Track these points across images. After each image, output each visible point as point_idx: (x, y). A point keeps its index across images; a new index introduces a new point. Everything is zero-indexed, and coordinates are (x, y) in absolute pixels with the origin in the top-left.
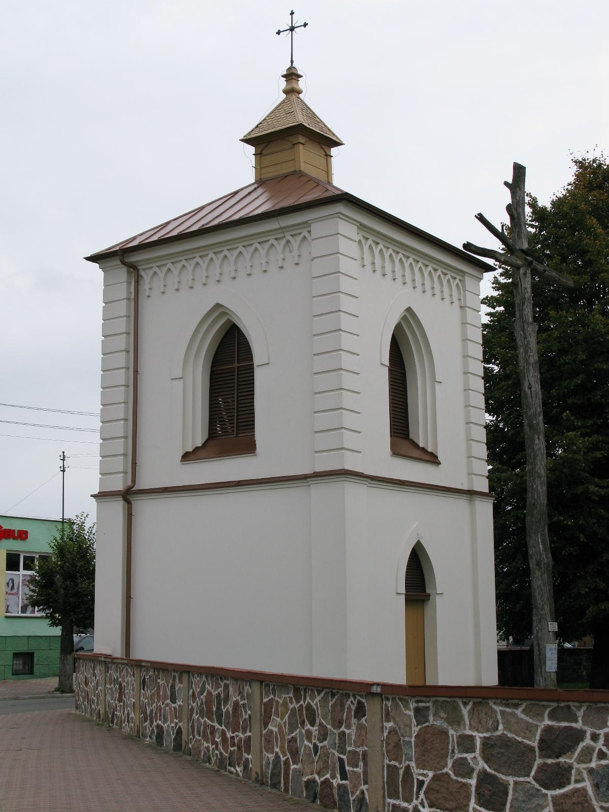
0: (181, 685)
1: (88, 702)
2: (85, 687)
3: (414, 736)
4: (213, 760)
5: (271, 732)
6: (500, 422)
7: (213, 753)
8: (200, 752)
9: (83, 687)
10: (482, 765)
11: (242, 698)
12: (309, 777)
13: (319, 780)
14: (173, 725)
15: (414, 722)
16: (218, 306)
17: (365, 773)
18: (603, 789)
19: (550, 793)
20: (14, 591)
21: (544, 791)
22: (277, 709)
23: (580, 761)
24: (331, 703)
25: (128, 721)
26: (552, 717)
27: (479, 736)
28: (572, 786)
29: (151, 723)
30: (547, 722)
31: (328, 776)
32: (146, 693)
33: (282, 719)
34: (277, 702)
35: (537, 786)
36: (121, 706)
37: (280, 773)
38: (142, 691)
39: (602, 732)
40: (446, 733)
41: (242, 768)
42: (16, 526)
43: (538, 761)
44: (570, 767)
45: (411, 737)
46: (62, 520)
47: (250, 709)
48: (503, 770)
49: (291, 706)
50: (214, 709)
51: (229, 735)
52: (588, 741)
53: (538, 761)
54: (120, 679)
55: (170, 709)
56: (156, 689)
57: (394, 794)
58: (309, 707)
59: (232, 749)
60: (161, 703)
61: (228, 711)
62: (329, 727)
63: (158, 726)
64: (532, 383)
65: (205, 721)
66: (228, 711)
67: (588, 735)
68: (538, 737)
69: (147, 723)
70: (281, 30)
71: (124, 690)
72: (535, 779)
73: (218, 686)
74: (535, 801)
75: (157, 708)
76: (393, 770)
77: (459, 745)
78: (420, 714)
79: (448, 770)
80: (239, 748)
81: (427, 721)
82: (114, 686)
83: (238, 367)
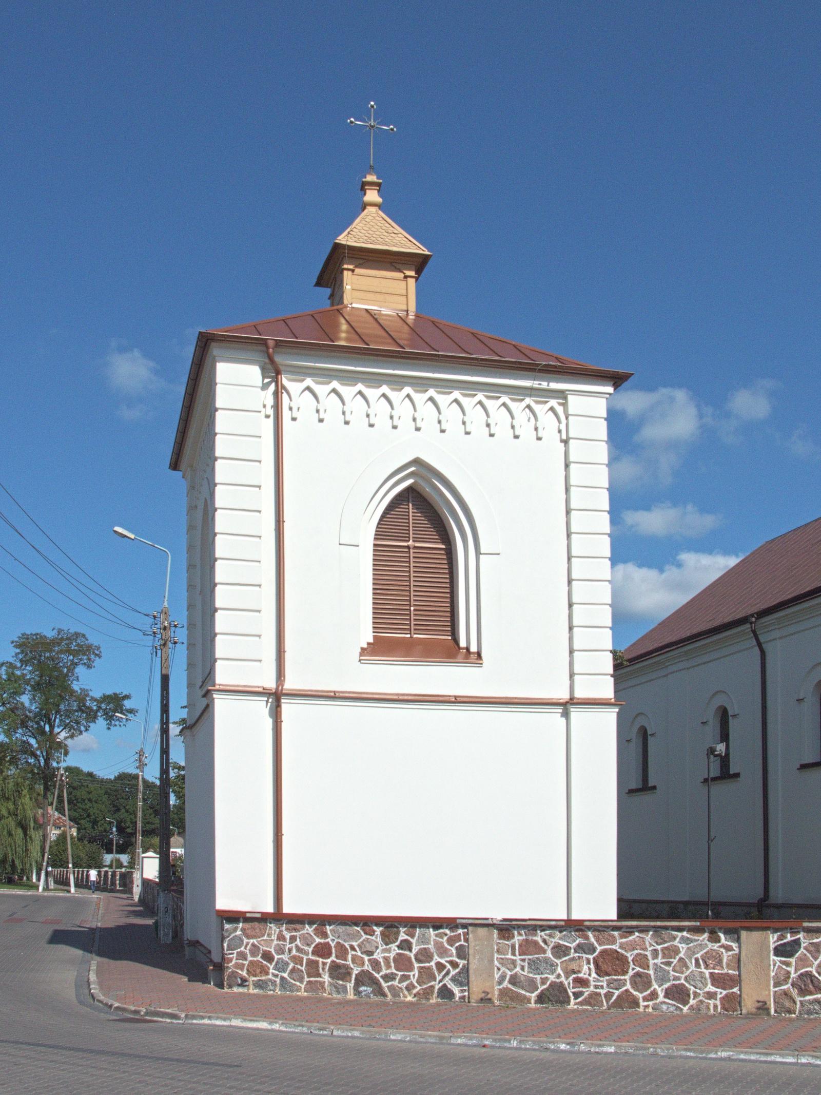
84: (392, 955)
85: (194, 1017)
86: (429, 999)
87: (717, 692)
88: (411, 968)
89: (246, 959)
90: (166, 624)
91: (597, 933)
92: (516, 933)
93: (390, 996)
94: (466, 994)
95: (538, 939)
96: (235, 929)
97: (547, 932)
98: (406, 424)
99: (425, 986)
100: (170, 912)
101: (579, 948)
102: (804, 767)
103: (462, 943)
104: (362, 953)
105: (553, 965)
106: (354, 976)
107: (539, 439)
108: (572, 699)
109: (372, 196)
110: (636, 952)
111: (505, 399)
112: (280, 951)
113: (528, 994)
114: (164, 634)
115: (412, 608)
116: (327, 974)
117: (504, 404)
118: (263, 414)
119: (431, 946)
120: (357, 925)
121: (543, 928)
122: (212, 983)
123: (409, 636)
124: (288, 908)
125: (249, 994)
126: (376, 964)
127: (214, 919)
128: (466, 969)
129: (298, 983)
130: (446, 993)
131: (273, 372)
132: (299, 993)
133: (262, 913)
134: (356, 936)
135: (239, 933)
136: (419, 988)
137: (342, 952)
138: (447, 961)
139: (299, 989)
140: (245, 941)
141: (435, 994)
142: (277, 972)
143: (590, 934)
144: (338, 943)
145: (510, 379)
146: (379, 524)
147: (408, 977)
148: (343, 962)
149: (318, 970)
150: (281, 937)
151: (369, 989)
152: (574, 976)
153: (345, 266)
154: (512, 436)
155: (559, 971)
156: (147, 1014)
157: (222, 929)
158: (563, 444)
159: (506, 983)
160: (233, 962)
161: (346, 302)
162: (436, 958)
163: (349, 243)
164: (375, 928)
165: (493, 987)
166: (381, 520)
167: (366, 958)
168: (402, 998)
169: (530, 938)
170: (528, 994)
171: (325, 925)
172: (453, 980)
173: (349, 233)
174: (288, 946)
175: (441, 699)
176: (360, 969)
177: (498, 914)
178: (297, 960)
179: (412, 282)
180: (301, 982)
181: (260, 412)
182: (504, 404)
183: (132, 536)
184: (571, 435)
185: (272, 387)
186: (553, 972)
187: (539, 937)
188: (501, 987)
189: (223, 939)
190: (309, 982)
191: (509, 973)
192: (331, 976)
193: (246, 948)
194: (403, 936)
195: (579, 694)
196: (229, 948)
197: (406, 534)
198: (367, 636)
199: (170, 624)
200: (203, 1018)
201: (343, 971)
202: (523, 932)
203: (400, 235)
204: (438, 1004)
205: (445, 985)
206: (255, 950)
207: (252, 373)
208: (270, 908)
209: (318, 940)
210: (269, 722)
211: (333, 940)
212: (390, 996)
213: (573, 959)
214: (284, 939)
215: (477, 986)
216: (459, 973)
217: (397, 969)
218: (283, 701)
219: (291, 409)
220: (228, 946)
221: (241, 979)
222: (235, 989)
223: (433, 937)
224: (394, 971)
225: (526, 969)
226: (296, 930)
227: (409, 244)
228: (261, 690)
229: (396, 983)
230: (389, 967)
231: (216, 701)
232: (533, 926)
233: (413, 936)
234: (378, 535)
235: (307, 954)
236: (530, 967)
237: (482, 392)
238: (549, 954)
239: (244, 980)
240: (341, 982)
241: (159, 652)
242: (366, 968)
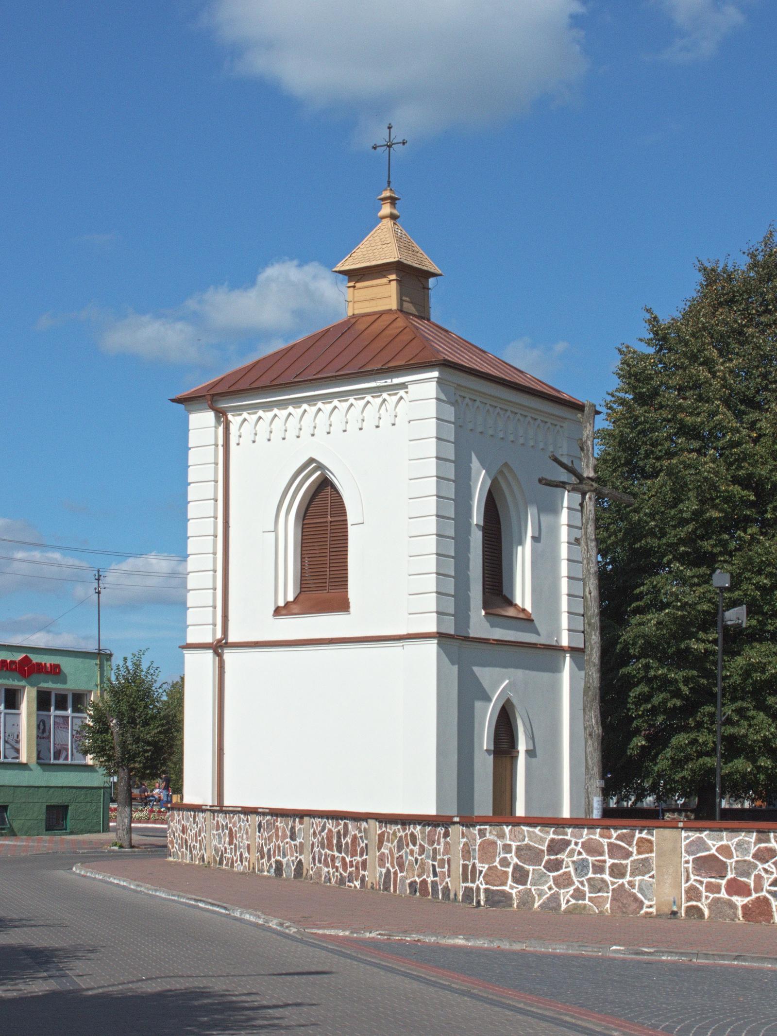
0: (302, 826)
1: (186, 849)
2: (181, 834)
3: (478, 844)
4: (333, 881)
5: (383, 854)
6: (608, 564)
7: (333, 875)
8: (321, 876)
9: (179, 835)
10: (516, 860)
11: (360, 832)
12: (412, 879)
13: (418, 880)
14: (294, 858)
15: (478, 837)
16: (311, 460)
17: (449, 871)
18: (579, 871)
19: (552, 874)
20: (45, 735)
21: (548, 873)
22: (388, 837)
23: (568, 856)
24: (427, 831)
25: (241, 861)
26: (554, 833)
27: (514, 845)
28: (564, 870)
29: (269, 859)
30: (552, 836)
31: (425, 877)
32: (262, 835)
33: (392, 844)
34: (388, 833)
35: (545, 871)
36: (231, 848)
37: (390, 880)
38: (258, 834)
39: (580, 841)
40: (495, 843)
41: (359, 882)
42: (47, 660)
43: (546, 858)
44: (563, 860)
45: (475, 845)
46: (96, 651)
47: (366, 839)
48: (527, 863)
49: (399, 835)
50: (335, 842)
51: (348, 859)
52: (572, 846)
53: (546, 858)
54: (231, 825)
55: (290, 846)
56: (274, 831)
57: (465, 880)
58: (412, 835)
59: (351, 870)
60: (279, 842)
61: (347, 843)
62: (426, 846)
63: (277, 862)
64: (592, 589)
65: (326, 853)
66: (347, 843)
67: (573, 843)
68: (546, 844)
69: (265, 860)
70: (378, 145)
71: (236, 835)
72: (544, 867)
73: (338, 825)
74: (544, 879)
75: (275, 847)
76: (465, 867)
77: (503, 849)
78: (482, 833)
79: (496, 864)
80: (357, 868)
81: (485, 836)
82: (223, 832)
83: (331, 522)
145: (364, 383)
207: (209, 416)
237: (353, 395)
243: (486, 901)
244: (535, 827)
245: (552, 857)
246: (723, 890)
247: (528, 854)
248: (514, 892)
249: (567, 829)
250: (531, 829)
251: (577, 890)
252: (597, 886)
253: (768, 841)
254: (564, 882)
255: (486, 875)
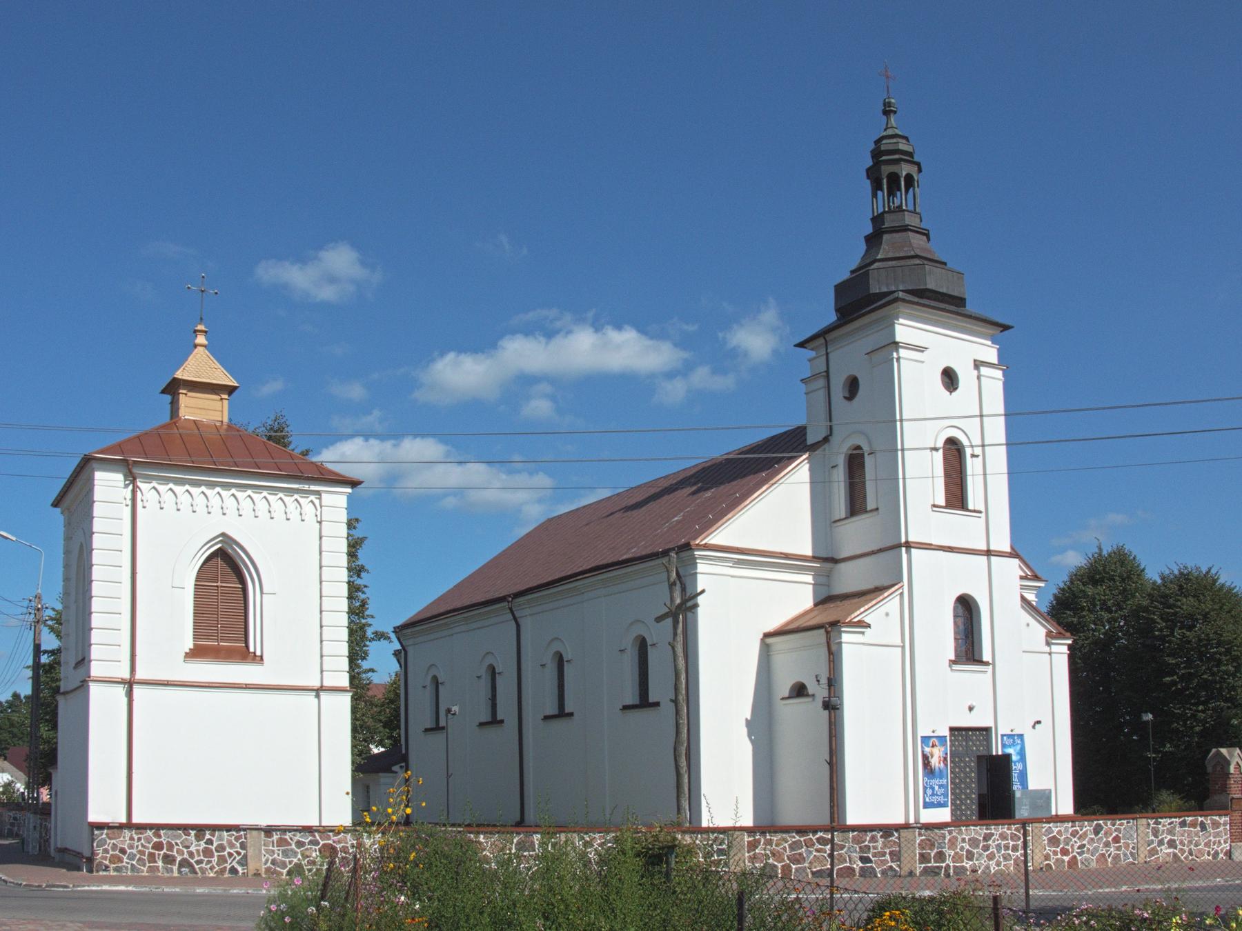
10: (968, 847)
78: (950, 833)
84: (201, 848)
85: (78, 886)
86: (223, 875)
87: (488, 653)
88: (212, 856)
89: (108, 853)
90: (40, 606)
91: (320, 834)
92: (274, 833)
93: (200, 874)
94: (246, 871)
95: (287, 837)
96: (102, 834)
97: (293, 833)
98: (216, 510)
99: (221, 867)
100: (38, 829)
101: (311, 842)
102: (546, 718)
103: (243, 840)
104: (183, 847)
105: (296, 853)
106: (177, 862)
107: (303, 520)
108: (322, 687)
109: (201, 339)
110: (342, 845)
111: (281, 495)
112: (131, 847)
113: (282, 870)
114: (37, 614)
115: (219, 626)
116: (161, 861)
117: (281, 499)
118: (124, 504)
119: (225, 842)
120: (179, 829)
121: (290, 831)
122: (85, 871)
123: (216, 643)
124: (136, 819)
125: (110, 875)
126: (191, 854)
127: (87, 828)
128: (245, 856)
129: (142, 868)
130: (233, 871)
131: (131, 478)
132: (143, 874)
133: (120, 823)
134: (179, 837)
135: (104, 836)
136: (217, 868)
137: (170, 847)
138: (235, 852)
139: (143, 871)
140: (108, 841)
141: (227, 872)
142: (128, 861)
143: (316, 834)
144: (168, 841)
146: (199, 571)
147: (210, 862)
148: (171, 853)
149: (155, 859)
150: (132, 839)
151: (187, 870)
152: (308, 859)
153: (181, 391)
154: (285, 518)
155: (299, 856)
156: (47, 886)
157: (93, 834)
158: (318, 524)
159: (269, 864)
160: (100, 855)
161: (180, 415)
162: (228, 850)
163: (184, 378)
164: (191, 831)
165: (261, 867)
166: (200, 569)
167: (185, 850)
168: (207, 875)
169: (283, 836)
170: (282, 870)
171: (159, 830)
172: (238, 862)
173: (184, 369)
174: (136, 844)
175: (236, 686)
176: (181, 857)
177: (264, 822)
178: (142, 853)
179: (226, 402)
180: (144, 867)
181: (122, 503)
182: (281, 499)
183: (14, 539)
184: (323, 519)
185: (131, 487)
186: (296, 857)
187: (288, 836)
188: (266, 866)
189: (93, 842)
190: (149, 867)
191: (271, 858)
192: (164, 862)
193: (108, 846)
194: (208, 836)
195: (326, 684)
196: (98, 846)
197: (215, 590)
198: (189, 644)
199: (42, 606)
200: (84, 886)
201: (171, 858)
202: (278, 833)
203: (219, 370)
204: (229, 877)
205: (233, 866)
206: (114, 847)
207: (118, 477)
208: (124, 820)
209: (155, 840)
210: (125, 700)
211: (165, 840)
212: (200, 874)
213: (307, 849)
214: (133, 839)
215: (252, 866)
216: (241, 858)
217: (204, 857)
218: (134, 687)
219: (142, 501)
220: (97, 845)
221: (105, 866)
222: (101, 873)
223: (226, 837)
224: (202, 858)
225: (281, 855)
226: (141, 833)
227: (224, 377)
228: (120, 680)
229: (203, 865)
230: (199, 855)
231: (91, 687)
232: (284, 830)
233: (213, 836)
234: (198, 579)
235: (148, 848)
236: (283, 854)
238: (293, 846)
239: (107, 868)
240: (169, 866)
241: (33, 628)
242: (185, 856)
243: (954, 872)
244: (977, 826)
245: (985, 843)
246: (1059, 854)
247: (974, 843)
248: (968, 866)
249: (962, 828)
250: (975, 828)
251: (997, 861)
252: (1006, 858)
253: (991, 829)
254: (991, 857)
255: (953, 857)
